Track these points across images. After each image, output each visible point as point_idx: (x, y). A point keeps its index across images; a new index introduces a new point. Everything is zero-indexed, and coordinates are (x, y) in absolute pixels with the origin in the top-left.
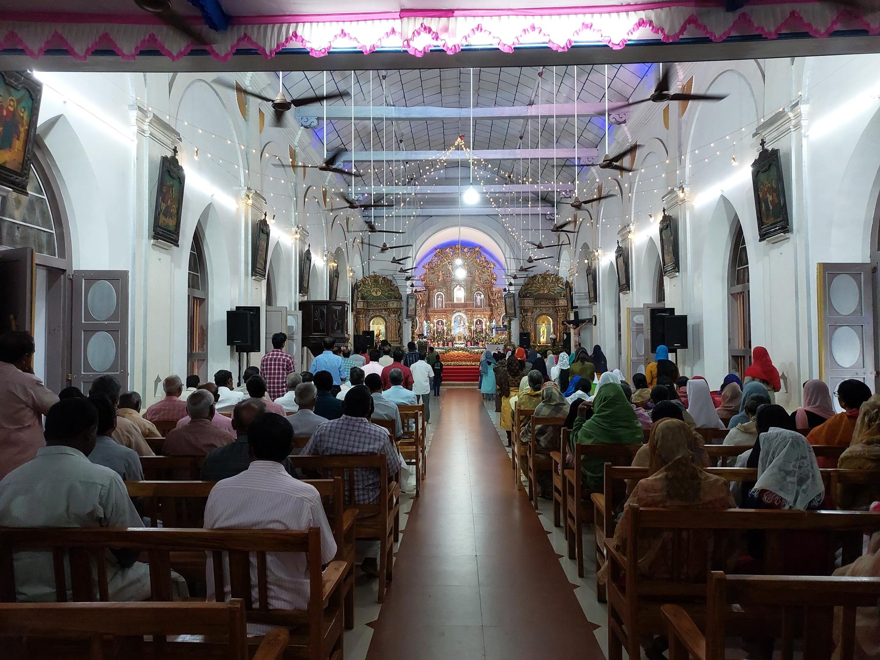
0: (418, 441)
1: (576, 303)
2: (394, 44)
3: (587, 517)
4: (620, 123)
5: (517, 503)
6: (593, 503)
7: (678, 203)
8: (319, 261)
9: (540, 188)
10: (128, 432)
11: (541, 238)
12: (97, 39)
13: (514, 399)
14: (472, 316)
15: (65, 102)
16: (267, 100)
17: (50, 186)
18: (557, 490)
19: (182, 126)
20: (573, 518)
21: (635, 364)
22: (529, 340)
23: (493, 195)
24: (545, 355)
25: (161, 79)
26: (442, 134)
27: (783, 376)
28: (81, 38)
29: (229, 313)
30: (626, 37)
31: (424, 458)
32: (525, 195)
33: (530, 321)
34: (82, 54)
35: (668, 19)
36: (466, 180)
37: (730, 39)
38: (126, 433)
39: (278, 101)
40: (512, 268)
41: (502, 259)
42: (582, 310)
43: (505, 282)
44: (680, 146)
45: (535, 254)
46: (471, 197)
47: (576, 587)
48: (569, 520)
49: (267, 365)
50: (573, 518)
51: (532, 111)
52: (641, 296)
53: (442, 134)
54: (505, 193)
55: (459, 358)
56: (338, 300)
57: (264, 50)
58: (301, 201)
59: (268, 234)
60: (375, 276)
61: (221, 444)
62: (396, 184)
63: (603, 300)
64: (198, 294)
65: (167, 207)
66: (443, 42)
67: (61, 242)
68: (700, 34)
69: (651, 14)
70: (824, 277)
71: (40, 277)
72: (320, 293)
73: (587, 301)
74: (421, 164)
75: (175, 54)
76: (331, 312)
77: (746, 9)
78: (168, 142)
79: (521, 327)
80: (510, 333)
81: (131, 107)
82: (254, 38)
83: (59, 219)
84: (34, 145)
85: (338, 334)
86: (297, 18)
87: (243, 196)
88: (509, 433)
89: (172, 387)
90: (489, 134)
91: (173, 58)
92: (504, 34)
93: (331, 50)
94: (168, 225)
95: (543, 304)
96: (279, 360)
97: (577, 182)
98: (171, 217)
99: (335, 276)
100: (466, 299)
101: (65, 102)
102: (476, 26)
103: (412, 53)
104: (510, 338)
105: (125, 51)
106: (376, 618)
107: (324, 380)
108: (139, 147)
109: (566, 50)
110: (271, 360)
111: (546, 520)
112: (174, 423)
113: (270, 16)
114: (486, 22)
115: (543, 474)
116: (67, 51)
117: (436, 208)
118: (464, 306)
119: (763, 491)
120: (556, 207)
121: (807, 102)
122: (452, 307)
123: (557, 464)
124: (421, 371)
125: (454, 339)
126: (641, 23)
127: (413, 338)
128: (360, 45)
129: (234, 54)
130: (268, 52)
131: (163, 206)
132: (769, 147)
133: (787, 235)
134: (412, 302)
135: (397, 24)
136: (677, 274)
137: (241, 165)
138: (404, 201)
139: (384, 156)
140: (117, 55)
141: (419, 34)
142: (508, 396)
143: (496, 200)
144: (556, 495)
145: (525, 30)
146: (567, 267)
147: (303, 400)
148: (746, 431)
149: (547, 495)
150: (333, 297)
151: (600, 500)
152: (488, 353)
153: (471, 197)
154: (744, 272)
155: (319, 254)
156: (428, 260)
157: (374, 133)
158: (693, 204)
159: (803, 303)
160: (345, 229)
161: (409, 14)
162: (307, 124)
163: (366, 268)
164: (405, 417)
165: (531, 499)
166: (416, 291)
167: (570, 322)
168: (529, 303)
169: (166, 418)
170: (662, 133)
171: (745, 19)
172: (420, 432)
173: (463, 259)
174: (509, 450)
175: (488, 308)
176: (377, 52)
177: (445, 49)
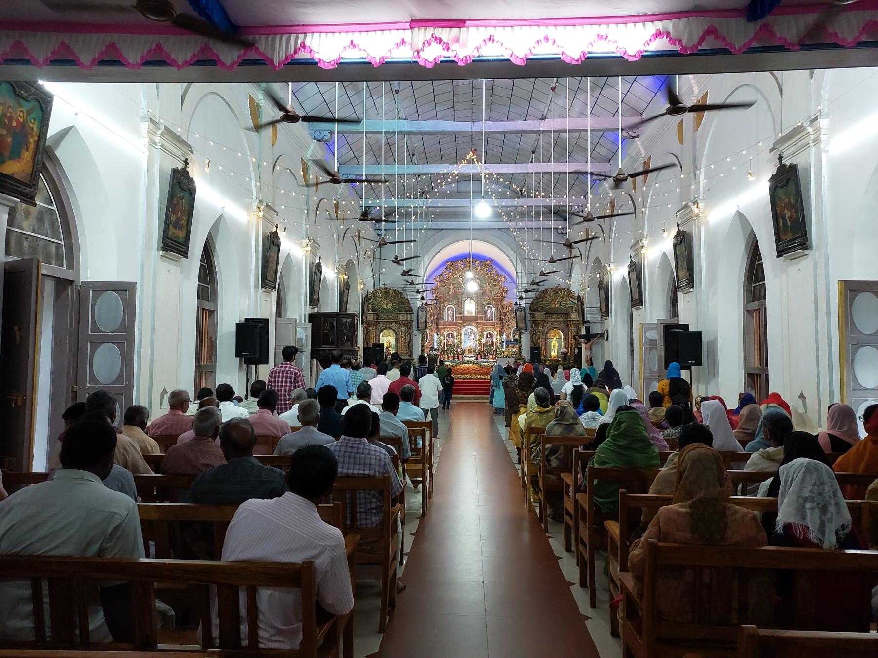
0: (425, 458)
1: (588, 317)
2: (404, 54)
4: (633, 138)
5: (526, 525)
8: (330, 273)
9: (553, 202)
10: (125, 450)
11: (553, 251)
12: (104, 49)
15: (76, 114)
17: (60, 197)
18: (568, 513)
20: (585, 546)
21: (648, 381)
22: (539, 354)
23: (504, 209)
25: (173, 90)
26: (455, 148)
28: (88, 48)
29: (238, 326)
30: (643, 48)
31: (431, 475)
32: (537, 209)
33: (540, 335)
34: (88, 63)
35: (687, 32)
36: (478, 194)
40: (524, 281)
41: (513, 273)
43: (516, 295)
44: (694, 160)
45: (547, 268)
46: (482, 210)
48: (580, 546)
49: (275, 377)
50: (585, 546)
51: (544, 125)
52: (654, 311)
53: (455, 148)
55: (469, 372)
56: (349, 312)
58: (312, 213)
59: (279, 247)
60: (386, 288)
62: (408, 198)
63: (616, 316)
64: (208, 305)
66: (454, 53)
67: (69, 252)
68: (719, 45)
69: (669, 25)
70: (846, 295)
71: (49, 287)
72: (331, 305)
74: (432, 178)
76: (340, 324)
77: (768, 19)
78: (180, 154)
80: (520, 347)
81: (143, 119)
84: (44, 157)
85: (347, 346)
86: (305, 28)
87: (254, 207)
89: (178, 401)
90: (501, 148)
91: (179, 67)
92: (517, 44)
93: (342, 61)
94: (177, 237)
96: (287, 373)
97: (590, 196)
98: (181, 228)
99: (345, 289)
100: (477, 312)
101: (76, 114)
102: (488, 36)
103: (422, 64)
104: (520, 352)
105: (131, 60)
107: (328, 394)
109: (580, 63)
110: (279, 372)
111: (557, 544)
112: (173, 438)
113: (275, 26)
114: (499, 33)
115: (553, 496)
118: (475, 319)
119: (788, 527)
120: (569, 224)
121: (826, 116)
122: (464, 320)
123: (568, 486)
124: (430, 386)
125: (464, 352)
127: (423, 351)
129: (241, 64)
130: (276, 63)
131: (173, 218)
132: (787, 162)
135: (407, 34)
136: (691, 290)
138: (416, 214)
139: (396, 169)
140: (123, 65)
141: (429, 44)
142: (517, 412)
143: (508, 214)
144: (567, 518)
146: (578, 281)
147: (305, 416)
148: (769, 457)
149: (558, 517)
151: (614, 528)
152: (500, 367)
153: (482, 210)
154: (760, 288)
155: (330, 267)
156: (439, 272)
157: (386, 147)
161: (419, 24)
162: (320, 138)
163: (377, 280)
164: (412, 434)
166: (426, 304)
167: (581, 337)
168: (540, 317)
169: (168, 432)
170: (676, 147)
171: (766, 28)
172: (427, 449)
173: (474, 272)
174: (518, 467)
176: (387, 63)
177: (455, 60)
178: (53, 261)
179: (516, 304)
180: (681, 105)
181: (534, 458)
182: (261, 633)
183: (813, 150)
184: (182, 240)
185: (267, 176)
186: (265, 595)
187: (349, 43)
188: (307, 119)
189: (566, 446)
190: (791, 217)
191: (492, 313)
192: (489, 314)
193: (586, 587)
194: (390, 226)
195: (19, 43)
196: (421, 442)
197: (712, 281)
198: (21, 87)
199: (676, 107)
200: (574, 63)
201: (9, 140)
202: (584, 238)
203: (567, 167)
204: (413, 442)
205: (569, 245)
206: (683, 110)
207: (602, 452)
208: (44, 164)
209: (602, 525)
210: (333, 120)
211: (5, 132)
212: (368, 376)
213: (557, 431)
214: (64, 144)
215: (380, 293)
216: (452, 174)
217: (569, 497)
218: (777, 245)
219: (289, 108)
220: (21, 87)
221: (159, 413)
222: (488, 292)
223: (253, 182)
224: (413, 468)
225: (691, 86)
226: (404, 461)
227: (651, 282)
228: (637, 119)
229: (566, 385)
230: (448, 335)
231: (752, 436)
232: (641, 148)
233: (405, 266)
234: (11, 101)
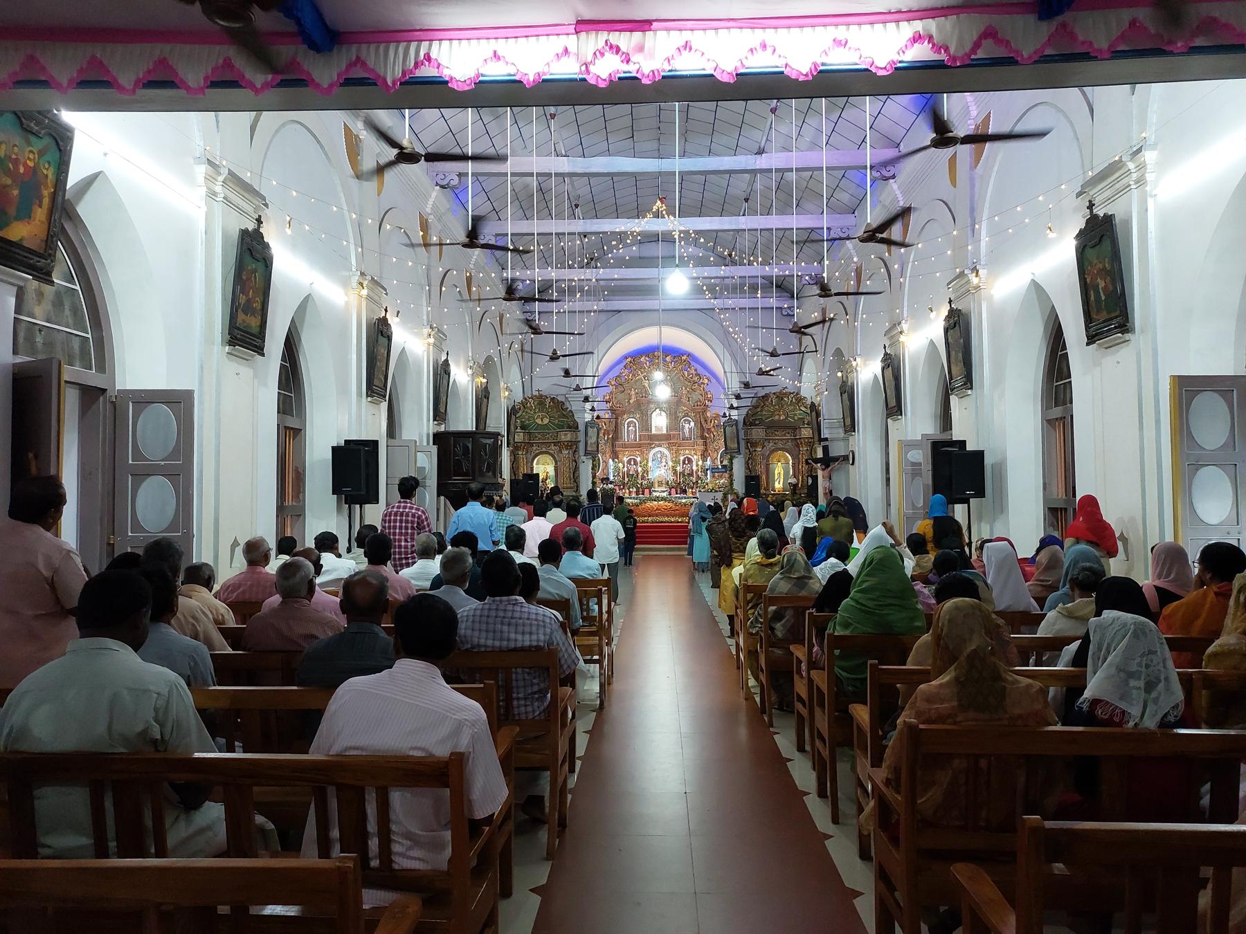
0: (601, 629)
1: (825, 433)
2: (567, 69)
3: (845, 733)
4: (887, 179)
5: (743, 717)
8: (461, 375)
10: (194, 617)
11: (776, 341)
13: (738, 570)
17: (84, 272)
18: (800, 699)
19: (269, 186)
20: (823, 740)
21: (910, 520)
22: (758, 486)
23: (707, 281)
26: (635, 195)
28: (128, 64)
30: (896, 58)
31: (611, 656)
32: (753, 281)
33: (759, 459)
34: (129, 86)
35: (955, 34)
36: (669, 260)
43: (725, 404)
44: (972, 210)
45: (767, 363)
46: (677, 284)
50: (823, 740)
51: (762, 162)
52: (918, 423)
53: (635, 195)
54: (724, 278)
57: (385, 80)
58: (436, 289)
59: (389, 339)
60: (541, 396)
61: (325, 634)
62: (570, 267)
64: (292, 422)
66: (637, 66)
67: (99, 348)
68: (1001, 52)
69: (931, 25)
70: (1180, 395)
71: (71, 402)
72: (463, 420)
73: (841, 431)
74: (605, 238)
77: (1067, 16)
78: (249, 209)
79: (748, 468)
80: (731, 476)
81: (198, 160)
82: (371, 63)
83: (97, 317)
84: (62, 213)
86: (430, 34)
87: (355, 284)
88: (731, 618)
89: (255, 553)
90: (702, 196)
91: (257, 92)
92: (723, 54)
95: (779, 435)
96: (407, 515)
97: (826, 262)
98: (253, 314)
99: (483, 397)
100: (669, 428)
102: (683, 43)
103: (592, 82)
104: (731, 484)
110: (396, 515)
111: (785, 742)
114: (698, 38)
115: (779, 678)
117: (626, 299)
118: (667, 437)
119: (1095, 702)
120: (798, 296)
121: (1153, 147)
122: (650, 440)
123: (799, 662)
124: (606, 530)
126: (917, 38)
127: (594, 483)
129: (341, 85)
130: (390, 83)
131: (243, 299)
133: (1127, 336)
135: (571, 41)
136: (969, 392)
137: (352, 241)
138: (581, 290)
139: (553, 226)
141: (602, 54)
142: (730, 565)
143: (711, 289)
144: (799, 706)
145: (751, 50)
146: (811, 382)
148: (1070, 615)
149: (785, 706)
150: (481, 427)
151: (862, 713)
152: (701, 504)
153: (677, 284)
154: (1065, 389)
155: (462, 366)
157: (539, 196)
158: (992, 292)
159: (1150, 433)
161: (590, 27)
163: (527, 385)
164: (584, 596)
165: (763, 711)
166: (598, 417)
167: (817, 461)
168: (758, 433)
169: (247, 596)
172: (605, 616)
174: (731, 642)
175: (700, 441)
176: (544, 81)
178: (78, 363)
179: (724, 416)
180: (950, 134)
181: (752, 625)
182: (396, 848)
183: (1135, 193)
184: (255, 330)
185: (371, 236)
186: (397, 797)
187: (491, 54)
188: (432, 157)
189: (795, 609)
190: (1106, 292)
191: (690, 429)
192: (687, 430)
193: (826, 797)
194: (546, 306)
195: (32, 59)
196: (596, 607)
197: (999, 379)
198: (31, 118)
199: (943, 136)
200: (801, 78)
201: (16, 192)
202: (819, 319)
203: (795, 221)
204: (585, 607)
205: (799, 331)
206: (952, 141)
207: (846, 610)
208: (63, 228)
209: (846, 711)
210: (464, 158)
211: (9, 182)
212: (516, 518)
213: (784, 587)
214: (88, 197)
216: (632, 233)
217: (802, 677)
218: (1087, 328)
219: (405, 143)
220: (31, 118)
221: (229, 568)
222: (684, 400)
223: (352, 247)
224: (586, 643)
225: (964, 109)
226: (575, 633)
227: (913, 386)
228: (891, 153)
229: (799, 521)
230: (629, 462)
231: (1054, 588)
232: (898, 192)
233: (566, 363)
234: (18, 140)
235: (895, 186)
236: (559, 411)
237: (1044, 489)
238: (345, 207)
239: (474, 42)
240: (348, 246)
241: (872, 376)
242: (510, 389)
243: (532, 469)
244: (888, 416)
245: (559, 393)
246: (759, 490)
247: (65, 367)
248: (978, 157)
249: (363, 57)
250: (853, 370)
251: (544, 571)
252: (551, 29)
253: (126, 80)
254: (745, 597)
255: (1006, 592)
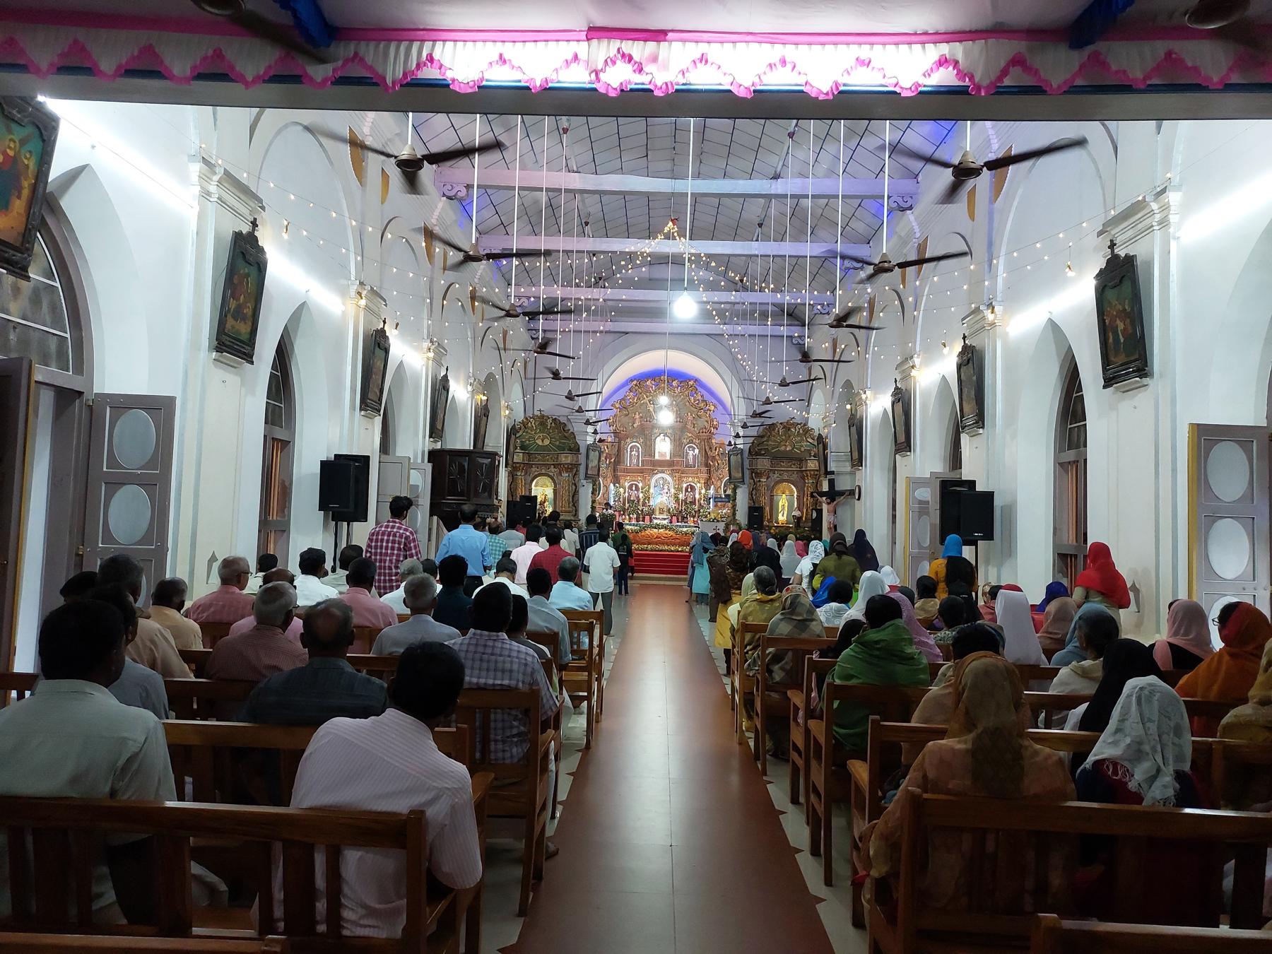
0: (592, 663)
1: (832, 466)
2: (576, 77)
3: (840, 791)
5: (735, 763)
6: (850, 775)
7: (983, 327)
8: (461, 393)
10: (153, 642)
13: (733, 610)
14: (680, 480)
16: (389, 156)
17: (65, 268)
18: (796, 748)
19: (266, 189)
20: (819, 795)
21: (916, 560)
23: (717, 306)
24: (781, 540)
25: (238, 117)
26: (646, 215)
27: (1134, 588)
28: (111, 51)
29: (324, 464)
31: (600, 690)
32: (763, 308)
36: (678, 283)
37: (1074, 90)
38: (148, 643)
39: (404, 157)
40: (741, 411)
41: (727, 401)
42: (841, 477)
43: (732, 433)
44: (990, 245)
45: (774, 393)
46: (685, 307)
47: (820, 900)
50: (819, 795)
51: (777, 187)
52: (927, 460)
53: (646, 215)
54: (734, 303)
55: (659, 540)
57: (384, 79)
59: (387, 351)
61: (288, 666)
62: (577, 285)
63: (872, 466)
64: (280, 434)
65: (239, 307)
66: (649, 77)
67: (78, 350)
68: (1028, 81)
69: (957, 50)
71: (46, 401)
72: (461, 438)
73: (848, 464)
75: (250, 78)
77: (1100, 46)
78: (245, 211)
79: (751, 498)
80: (734, 506)
81: (192, 158)
82: (369, 60)
83: (77, 317)
84: (44, 210)
87: (353, 293)
88: (727, 652)
89: (233, 573)
90: (712, 219)
92: (740, 68)
93: (484, 83)
96: (395, 535)
97: (839, 292)
99: (483, 415)
100: (673, 455)
101: (93, 147)
103: (602, 90)
104: (734, 514)
105: (177, 71)
106: (514, 940)
108: (201, 216)
110: (383, 534)
111: (778, 792)
114: (715, 51)
115: (775, 723)
116: (90, 70)
117: (633, 321)
118: (670, 464)
121: (1178, 188)
122: (652, 466)
123: (797, 709)
125: (653, 511)
126: (943, 62)
127: (593, 508)
128: (526, 78)
130: (389, 81)
131: (233, 304)
132: (1121, 252)
133: (1145, 381)
134: (594, 455)
135: (582, 48)
136: (981, 431)
137: (352, 249)
138: (588, 310)
140: (166, 78)
141: (614, 63)
143: (721, 314)
144: (794, 755)
145: (770, 65)
146: (820, 414)
148: (1084, 674)
149: (780, 754)
150: (479, 445)
151: (860, 771)
152: (704, 534)
155: (462, 382)
157: (549, 210)
158: (1008, 329)
159: (1165, 482)
160: (501, 346)
161: (601, 34)
162: (451, 194)
163: (529, 404)
164: (574, 628)
165: (757, 758)
167: (822, 494)
168: (763, 463)
171: (1097, 61)
172: (596, 651)
174: (727, 680)
175: (704, 469)
176: (551, 89)
178: (54, 363)
179: (730, 444)
184: (245, 337)
186: (353, 860)
187: (497, 58)
189: (795, 651)
191: (694, 456)
196: (587, 640)
197: (1011, 419)
212: (512, 542)
213: (785, 629)
215: (533, 423)
216: (642, 253)
217: (798, 724)
223: (352, 256)
235: (912, 218)
236: (560, 432)
237: (1055, 534)
238: (347, 214)
239: (479, 44)
240: (347, 256)
241: (881, 410)
242: (511, 407)
243: (530, 490)
244: (897, 451)
245: (561, 413)
246: (762, 521)
247: (37, 366)
248: (997, 188)
249: (362, 53)
250: (863, 403)
251: (533, 603)
252: (561, 35)
253: (107, 65)
254: (743, 639)
255: (1022, 645)
